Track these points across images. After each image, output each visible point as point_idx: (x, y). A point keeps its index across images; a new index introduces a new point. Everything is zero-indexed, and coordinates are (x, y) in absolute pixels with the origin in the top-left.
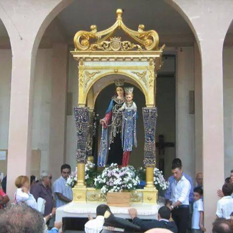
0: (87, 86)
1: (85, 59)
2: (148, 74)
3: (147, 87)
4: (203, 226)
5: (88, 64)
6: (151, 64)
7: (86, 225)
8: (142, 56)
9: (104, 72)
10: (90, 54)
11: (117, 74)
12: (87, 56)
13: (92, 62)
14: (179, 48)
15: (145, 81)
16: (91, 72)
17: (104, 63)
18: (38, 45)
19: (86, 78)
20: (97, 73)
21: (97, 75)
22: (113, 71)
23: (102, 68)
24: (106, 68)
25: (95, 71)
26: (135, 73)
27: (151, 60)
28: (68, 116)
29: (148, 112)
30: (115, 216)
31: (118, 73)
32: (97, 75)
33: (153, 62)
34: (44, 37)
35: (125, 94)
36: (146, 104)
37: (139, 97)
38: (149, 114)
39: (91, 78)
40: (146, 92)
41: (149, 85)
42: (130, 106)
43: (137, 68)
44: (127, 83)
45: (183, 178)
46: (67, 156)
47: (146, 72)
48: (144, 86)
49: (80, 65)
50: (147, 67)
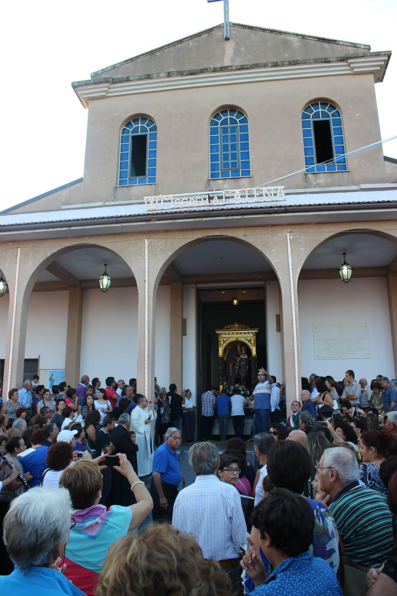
1: (221, 334)
5: (222, 336)
7: (72, 387)
9: (231, 340)
14: (267, 282)
16: (225, 340)
18: (158, 283)
21: (227, 341)
23: (230, 338)
28: (184, 337)
30: (344, 437)
32: (227, 341)
34: (163, 277)
35: (241, 350)
37: (248, 351)
43: (247, 337)
44: (243, 344)
45: (327, 549)
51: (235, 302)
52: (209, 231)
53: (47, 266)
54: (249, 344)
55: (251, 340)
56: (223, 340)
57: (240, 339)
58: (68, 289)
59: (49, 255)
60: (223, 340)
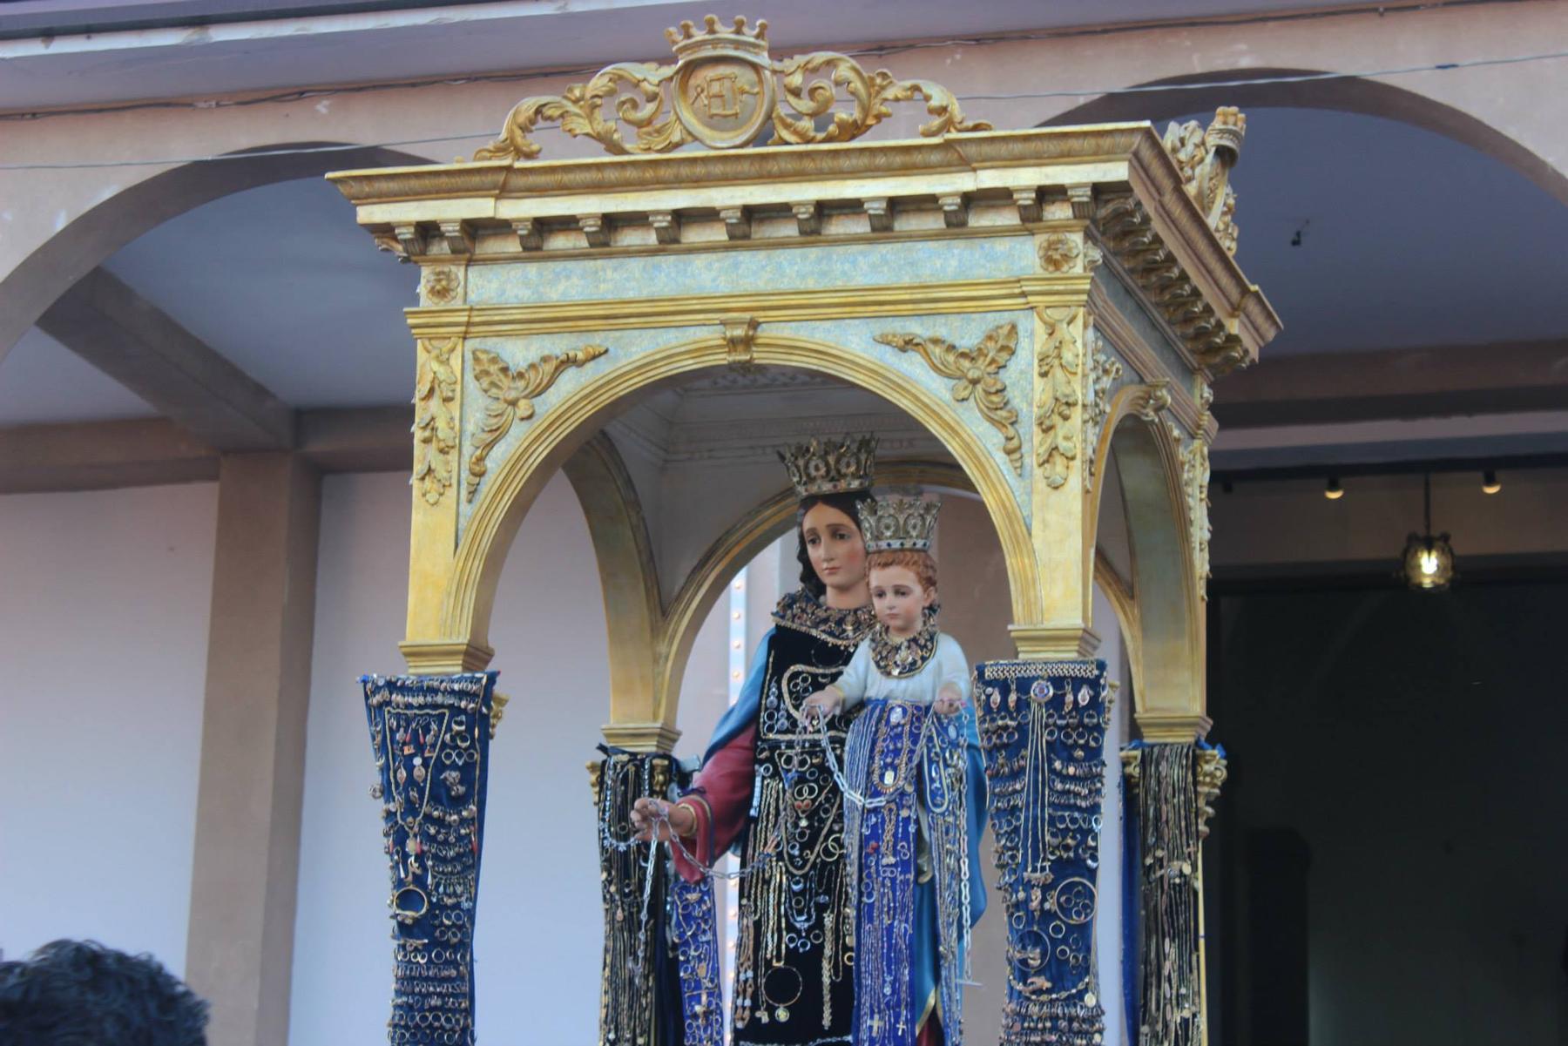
0: (488, 485)
2: (1032, 340)
3: (1020, 470)
4: (624, 752)
5: (495, 285)
6: (1054, 259)
8: (967, 182)
9: (637, 354)
10: (503, 192)
11: (746, 368)
12: (482, 208)
13: (532, 269)
15: (999, 410)
16: (520, 352)
17: (635, 265)
19: (477, 410)
20: (570, 362)
21: (570, 384)
22: (710, 335)
23: (614, 317)
24: (653, 315)
25: (559, 346)
26: (909, 344)
27: (1058, 212)
29: (1023, 705)
31: (760, 357)
33: (1076, 239)
36: (1017, 626)
38: (1037, 713)
39: (523, 408)
40: (1010, 517)
41: (1035, 443)
42: (910, 669)
43: (927, 301)
46: (15, 28)
47: (1014, 328)
48: (1000, 457)
49: (426, 302)
50: (1017, 289)
51: (1429, 565)
52: (1185, 39)
53: (49, 301)
54: (969, 435)
55: (1005, 344)
56: (493, 372)
57: (797, 341)
58: (213, 477)
59: (61, 223)
60: (493, 372)
